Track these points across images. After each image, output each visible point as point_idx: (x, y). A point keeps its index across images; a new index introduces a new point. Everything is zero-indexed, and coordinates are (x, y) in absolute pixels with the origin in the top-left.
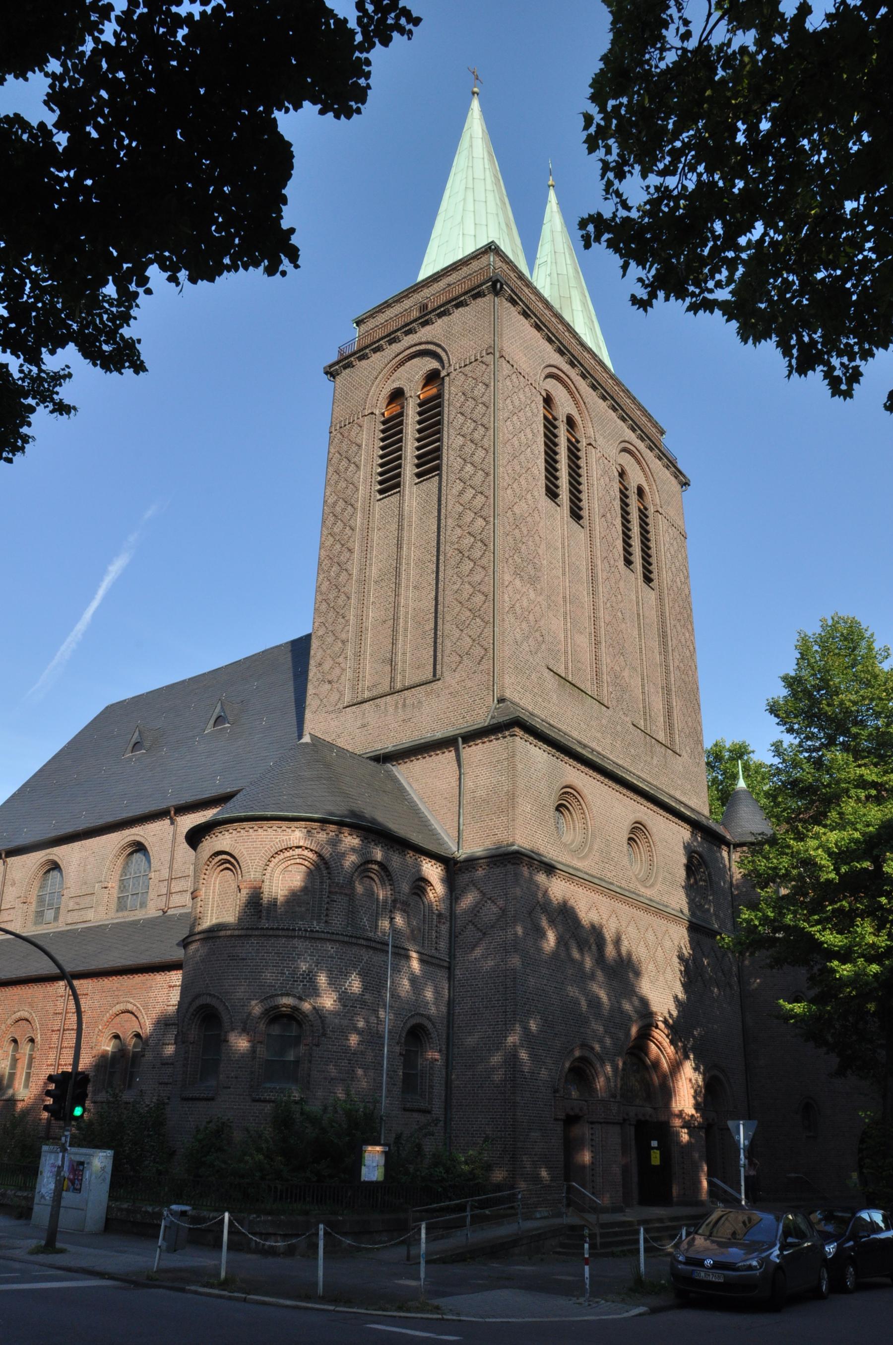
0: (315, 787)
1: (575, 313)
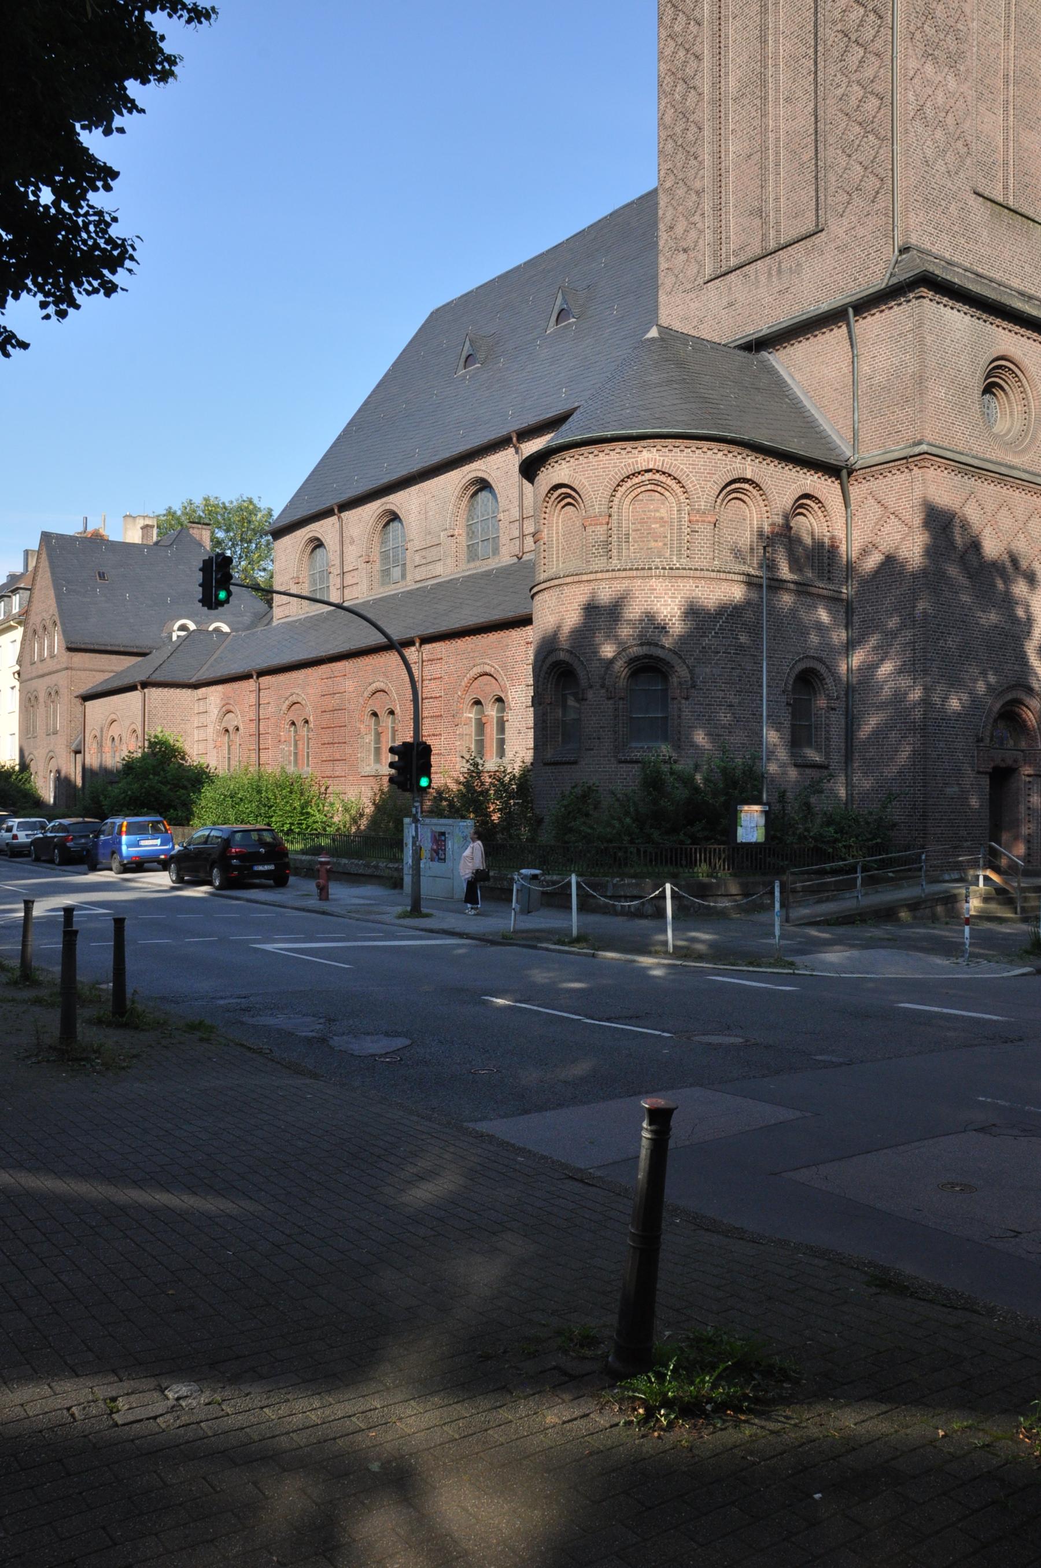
0: (665, 394)
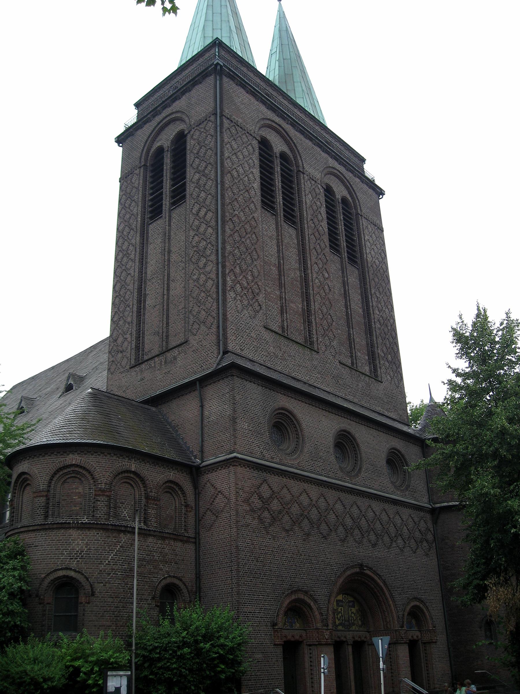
1: (296, 84)
